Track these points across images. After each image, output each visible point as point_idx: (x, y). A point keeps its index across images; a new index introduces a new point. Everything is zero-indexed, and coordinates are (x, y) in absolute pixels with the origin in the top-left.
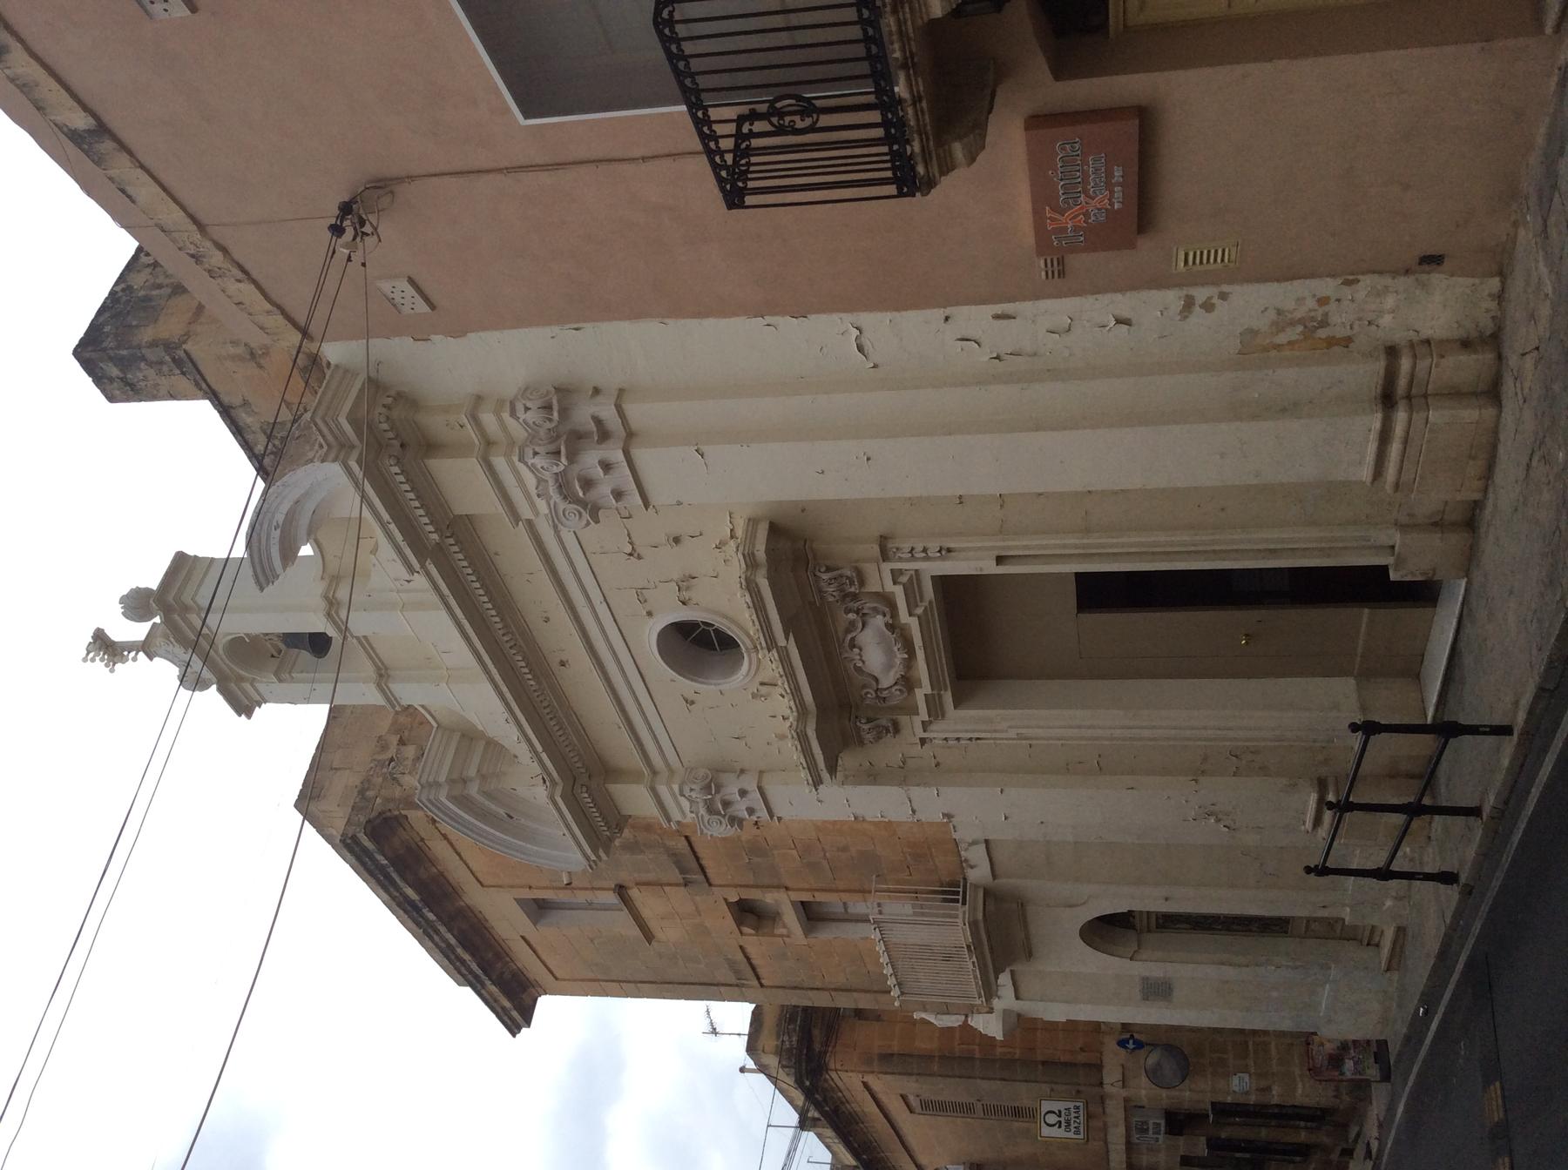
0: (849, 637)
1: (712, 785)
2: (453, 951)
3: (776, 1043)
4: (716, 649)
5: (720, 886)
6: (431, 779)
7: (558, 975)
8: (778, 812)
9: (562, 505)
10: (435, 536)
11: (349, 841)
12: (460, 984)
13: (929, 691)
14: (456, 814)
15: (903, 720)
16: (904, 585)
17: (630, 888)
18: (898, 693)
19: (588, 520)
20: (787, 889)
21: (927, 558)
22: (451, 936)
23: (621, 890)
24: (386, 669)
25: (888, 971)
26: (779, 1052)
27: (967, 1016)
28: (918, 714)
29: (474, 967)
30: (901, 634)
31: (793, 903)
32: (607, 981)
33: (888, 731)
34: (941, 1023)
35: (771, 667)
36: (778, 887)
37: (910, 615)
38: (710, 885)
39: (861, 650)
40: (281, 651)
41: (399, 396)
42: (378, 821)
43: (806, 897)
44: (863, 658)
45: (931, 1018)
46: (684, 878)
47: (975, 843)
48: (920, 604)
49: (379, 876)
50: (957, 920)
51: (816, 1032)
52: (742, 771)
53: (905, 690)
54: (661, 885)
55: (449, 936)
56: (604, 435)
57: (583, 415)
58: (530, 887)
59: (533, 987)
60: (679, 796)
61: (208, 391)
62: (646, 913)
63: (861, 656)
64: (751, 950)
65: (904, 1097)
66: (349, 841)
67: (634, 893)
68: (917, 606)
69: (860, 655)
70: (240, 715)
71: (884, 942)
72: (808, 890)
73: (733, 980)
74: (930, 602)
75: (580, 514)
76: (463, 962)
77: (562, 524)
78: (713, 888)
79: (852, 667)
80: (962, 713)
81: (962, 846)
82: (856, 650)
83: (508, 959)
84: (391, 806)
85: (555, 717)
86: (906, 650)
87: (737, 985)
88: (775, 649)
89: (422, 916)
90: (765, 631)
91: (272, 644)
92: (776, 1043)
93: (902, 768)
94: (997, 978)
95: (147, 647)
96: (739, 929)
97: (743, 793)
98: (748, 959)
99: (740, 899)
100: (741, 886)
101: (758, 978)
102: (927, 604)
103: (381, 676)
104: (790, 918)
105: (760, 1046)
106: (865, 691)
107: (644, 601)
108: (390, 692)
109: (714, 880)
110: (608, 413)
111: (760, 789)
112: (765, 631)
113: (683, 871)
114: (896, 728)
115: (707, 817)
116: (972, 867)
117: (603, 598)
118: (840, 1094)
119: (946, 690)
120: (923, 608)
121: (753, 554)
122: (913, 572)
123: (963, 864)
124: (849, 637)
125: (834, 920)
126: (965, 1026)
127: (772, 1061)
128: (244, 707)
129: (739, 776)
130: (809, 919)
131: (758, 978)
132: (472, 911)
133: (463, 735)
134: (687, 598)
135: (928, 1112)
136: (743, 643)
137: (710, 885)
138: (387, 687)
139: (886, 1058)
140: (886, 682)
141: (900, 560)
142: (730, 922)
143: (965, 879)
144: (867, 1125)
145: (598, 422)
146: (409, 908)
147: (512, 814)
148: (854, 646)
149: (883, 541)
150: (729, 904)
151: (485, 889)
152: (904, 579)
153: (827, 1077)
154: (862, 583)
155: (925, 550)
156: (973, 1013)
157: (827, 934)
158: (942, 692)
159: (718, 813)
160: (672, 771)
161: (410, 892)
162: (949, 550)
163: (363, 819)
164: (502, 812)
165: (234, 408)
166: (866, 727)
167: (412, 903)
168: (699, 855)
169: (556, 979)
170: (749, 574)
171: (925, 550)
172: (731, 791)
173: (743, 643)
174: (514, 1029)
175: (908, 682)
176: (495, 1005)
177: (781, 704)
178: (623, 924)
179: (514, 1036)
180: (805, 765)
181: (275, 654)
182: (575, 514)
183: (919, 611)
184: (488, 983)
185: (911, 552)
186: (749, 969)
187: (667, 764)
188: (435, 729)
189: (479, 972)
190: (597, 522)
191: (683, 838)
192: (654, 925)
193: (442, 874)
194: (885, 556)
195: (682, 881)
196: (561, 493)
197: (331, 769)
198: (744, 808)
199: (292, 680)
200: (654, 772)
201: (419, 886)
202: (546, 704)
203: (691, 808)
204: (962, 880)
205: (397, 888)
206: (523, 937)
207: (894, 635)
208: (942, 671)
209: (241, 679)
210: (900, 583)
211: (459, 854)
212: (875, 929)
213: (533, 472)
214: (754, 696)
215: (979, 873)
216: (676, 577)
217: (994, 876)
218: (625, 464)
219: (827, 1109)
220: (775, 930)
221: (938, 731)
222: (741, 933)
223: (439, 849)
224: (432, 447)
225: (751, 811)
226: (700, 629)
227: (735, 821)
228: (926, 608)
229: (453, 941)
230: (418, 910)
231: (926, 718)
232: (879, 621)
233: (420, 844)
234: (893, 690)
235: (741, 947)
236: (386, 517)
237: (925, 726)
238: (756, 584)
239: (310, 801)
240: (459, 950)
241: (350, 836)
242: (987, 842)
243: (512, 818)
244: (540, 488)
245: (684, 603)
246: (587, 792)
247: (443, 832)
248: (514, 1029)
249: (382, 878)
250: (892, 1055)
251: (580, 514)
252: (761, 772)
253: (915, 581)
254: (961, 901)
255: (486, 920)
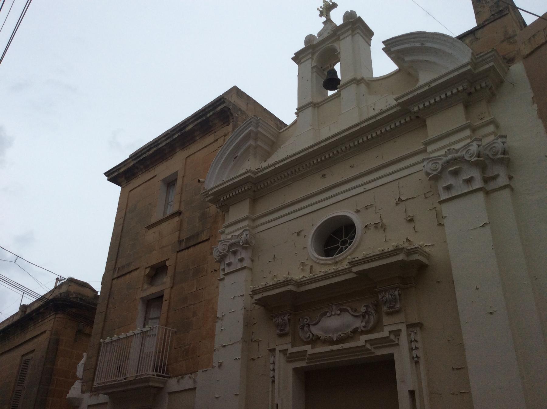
0: (349, 309)
1: (247, 245)
2: (155, 146)
3: (72, 292)
4: (325, 248)
5: (177, 257)
6: (260, 124)
7: (132, 192)
8: (227, 279)
9: (441, 162)
10: (416, 109)
11: (222, 100)
12: (130, 156)
13: (309, 353)
14: (240, 135)
15: (289, 339)
16: (364, 346)
17: (179, 218)
18: (308, 336)
19: (431, 174)
20: (172, 288)
21: (411, 349)
22: (163, 145)
23: (179, 213)
24: (318, 107)
25: (115, 337)
26: (68, 293)
27: (81, 379)
28: (292, 347)
29: (145, 156)
30: (349, 336)
31: (163, 291)
32: (126, 211)
33: (281, 330)
34: (80, 366)
35: (320, 271)
36: (173, 283)
37: (389, 332)
38: (178, 252)
39: (339, 315)
40: (324, 71)
41: (493, 95)
42: (229, 113)
43: (166, 297)
44: (332, 317)
45: (83, 361)
46: (183, 240)
47: (195, 382)
48: (372, 347)
49: (202, 114)
50: (151, 371)
51: (74, 310)
52: (252, 261)
53: (309, 339)
54: (180, 230)
55: (164, 144)
56: (486, 180)
57: (501, 171)
58: (184, 176)
59: (127, 183)
60: (244, 229)
61: (484, 24)
62: (164, 225)
63: (334, 315)
64: (41, 338)
65: (33, 351)
66: (222, 100)
67: (177, 219)
68: (371, 345)
69: (335, 314)
70: (295, 54)
71: (133, 335)
72: (170, 298)
73: (119, 265)
74: (374, 353)
75: (434, 170)
76: (148, 151)
77: (428, 162)
78: (176, 253)
79: (327, 311)
80: (291, 373)
81: (193, 376)
82: (339, 312)
83: (144, 171)
84: (235, 119)
85: (292, 173)
86: (338, 339)
87: (115, 268)
88: (351, 266)
89: (177, 132)
90: (365, 260)
91: (329, 66)
92: (72, 292)
93: (251, 341)
94: (106, 394)
95: (328, 21)
96: (148, 267)
97: (241, 260)
98: (130, 272)
99: (167, 267)
100: (175, 266)
101: (118, 278)
102: (373, 350)
103: (315, 105)
104: (153, 290)
105: (72, 284)
106: (308, 319)
107: (366, 208)
108: (308, 108)
109: (179, 254)
110: (502, 181)
111: (244, 268)
112: (365, 260)
113: (187, 239)
114: (282, 335)
115: (228, 244)
116: (178, 381)
117: (367, 189)
118: (40, 321)
119: (307, 363)
120: (394, 340)
121: (417, 253)
122: (397, 342)
123: (180, 376)
124: (349, 309)
125: (146, 311)
126: (75, 378)
127: (64, 290)
128: (298, 58)
129: (250, 258)
130: (148, 301)
131: (118, 278)
132: (172, 155)
133: (274, 143)
134: (370, 228)
135: (22, 364)
136: (340, 256)
137: (178, 252)
138: (310, 106)
139: (57, 342)
140: (315, 330)
141: (408, 335)
142: (154, 262)
143: (169, 377)
144: (19, 335)
145: (494, 178)
146: (182, 127)
147: (237, 159)
148: (341, 311)
149: (419, 325)
150: (165, 261)
151: (185, 159)
152: (392, 337)
153: (52, 314)
154: (389, 314)
155: (417, 348)
156: (83, 383)
157: (140, 308)
158: (306, 361)
159: (229, 249)
160: (253, 228)
161: (191, 127)
162: (417, 363)
163: (231, 107)
164: (239, 154)
165: (474, 35)
166: (286, 318)
167: (185, 127)
168: (196, 247)
169: (130, 191)
170: (405, 250)
171: (417, 348)
172: (243, 254)
173: (340, 256)
174: (107, 174)
175: (315, 341)
176: (123, 165)
177: (298, 275)
178: (158, 215)
179: (105, 174)
180: (267, 285)
181: (322, 68)
182: (435, 168)
183: (368, 346)
184: (135, 162)
185: (415, 340)
186: (124, 273)
187: (259, 226)
188: (279, 131)
189: (141, 158)
190: (430, 179)
191: (208, 238)
192: (156, 229)
193: (195, 141)
194: (409, 326)
195: (181, 239)
196: (451, 160)
197: (247, 103)
198: (231, 261)
199: (313, 73)
200: (254, 220)
201: (192, 131)
202: (301, 169)
203: (235, 235)
204: (169, 376)
205: (192, 122)
206: (156, 176)
207: (350, 333)
208: (327, 360)
209: (313, 54)
210: (390, 334)
211: (205, 147)
212: (150, 328)
213: (463, 147)
214: (303, 264)
215: (173, 385)
216: (384, 221)
217: (170, 393)
218: (471, 189)
219: (34, 315)
220: (146, 284)
221: (280, 359)
222: (146, 268)
223: (210, 139)
224: (467, 107)
225: (229, 265)
226: (344, 237)
227: (223, 257)
228: (370, 350)
229: (160, 146)
230: (180, 130)
231: (289, 352)
232: (359, 324)
233: (213, 132)
234: (310, 334)
235: (139, 268)
236: (433, 85)
237: (284, 352)
238: (398, 254)
239: (235, 91)
240: (155, 149)
241: (225, 100)
242: (195, 389)
243: (235, 158)
244: (454, 151)
245: (366, 226)
246: (248, 188)
247: (219, 140)
248: (107, 174)
249: (200, 115)
250: (58, 345)
251: (434, 170)
252: (251, 269)
253: (392, 343)
254: (160, 374)
255: (167, 161)
